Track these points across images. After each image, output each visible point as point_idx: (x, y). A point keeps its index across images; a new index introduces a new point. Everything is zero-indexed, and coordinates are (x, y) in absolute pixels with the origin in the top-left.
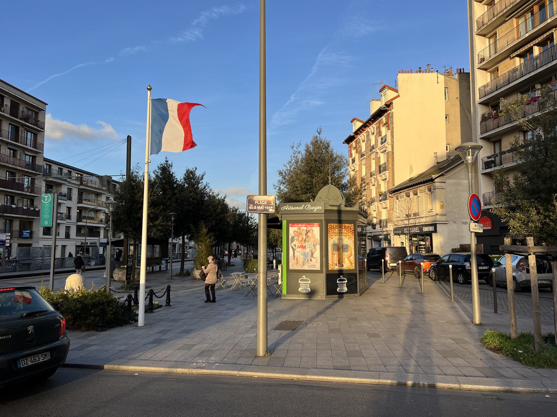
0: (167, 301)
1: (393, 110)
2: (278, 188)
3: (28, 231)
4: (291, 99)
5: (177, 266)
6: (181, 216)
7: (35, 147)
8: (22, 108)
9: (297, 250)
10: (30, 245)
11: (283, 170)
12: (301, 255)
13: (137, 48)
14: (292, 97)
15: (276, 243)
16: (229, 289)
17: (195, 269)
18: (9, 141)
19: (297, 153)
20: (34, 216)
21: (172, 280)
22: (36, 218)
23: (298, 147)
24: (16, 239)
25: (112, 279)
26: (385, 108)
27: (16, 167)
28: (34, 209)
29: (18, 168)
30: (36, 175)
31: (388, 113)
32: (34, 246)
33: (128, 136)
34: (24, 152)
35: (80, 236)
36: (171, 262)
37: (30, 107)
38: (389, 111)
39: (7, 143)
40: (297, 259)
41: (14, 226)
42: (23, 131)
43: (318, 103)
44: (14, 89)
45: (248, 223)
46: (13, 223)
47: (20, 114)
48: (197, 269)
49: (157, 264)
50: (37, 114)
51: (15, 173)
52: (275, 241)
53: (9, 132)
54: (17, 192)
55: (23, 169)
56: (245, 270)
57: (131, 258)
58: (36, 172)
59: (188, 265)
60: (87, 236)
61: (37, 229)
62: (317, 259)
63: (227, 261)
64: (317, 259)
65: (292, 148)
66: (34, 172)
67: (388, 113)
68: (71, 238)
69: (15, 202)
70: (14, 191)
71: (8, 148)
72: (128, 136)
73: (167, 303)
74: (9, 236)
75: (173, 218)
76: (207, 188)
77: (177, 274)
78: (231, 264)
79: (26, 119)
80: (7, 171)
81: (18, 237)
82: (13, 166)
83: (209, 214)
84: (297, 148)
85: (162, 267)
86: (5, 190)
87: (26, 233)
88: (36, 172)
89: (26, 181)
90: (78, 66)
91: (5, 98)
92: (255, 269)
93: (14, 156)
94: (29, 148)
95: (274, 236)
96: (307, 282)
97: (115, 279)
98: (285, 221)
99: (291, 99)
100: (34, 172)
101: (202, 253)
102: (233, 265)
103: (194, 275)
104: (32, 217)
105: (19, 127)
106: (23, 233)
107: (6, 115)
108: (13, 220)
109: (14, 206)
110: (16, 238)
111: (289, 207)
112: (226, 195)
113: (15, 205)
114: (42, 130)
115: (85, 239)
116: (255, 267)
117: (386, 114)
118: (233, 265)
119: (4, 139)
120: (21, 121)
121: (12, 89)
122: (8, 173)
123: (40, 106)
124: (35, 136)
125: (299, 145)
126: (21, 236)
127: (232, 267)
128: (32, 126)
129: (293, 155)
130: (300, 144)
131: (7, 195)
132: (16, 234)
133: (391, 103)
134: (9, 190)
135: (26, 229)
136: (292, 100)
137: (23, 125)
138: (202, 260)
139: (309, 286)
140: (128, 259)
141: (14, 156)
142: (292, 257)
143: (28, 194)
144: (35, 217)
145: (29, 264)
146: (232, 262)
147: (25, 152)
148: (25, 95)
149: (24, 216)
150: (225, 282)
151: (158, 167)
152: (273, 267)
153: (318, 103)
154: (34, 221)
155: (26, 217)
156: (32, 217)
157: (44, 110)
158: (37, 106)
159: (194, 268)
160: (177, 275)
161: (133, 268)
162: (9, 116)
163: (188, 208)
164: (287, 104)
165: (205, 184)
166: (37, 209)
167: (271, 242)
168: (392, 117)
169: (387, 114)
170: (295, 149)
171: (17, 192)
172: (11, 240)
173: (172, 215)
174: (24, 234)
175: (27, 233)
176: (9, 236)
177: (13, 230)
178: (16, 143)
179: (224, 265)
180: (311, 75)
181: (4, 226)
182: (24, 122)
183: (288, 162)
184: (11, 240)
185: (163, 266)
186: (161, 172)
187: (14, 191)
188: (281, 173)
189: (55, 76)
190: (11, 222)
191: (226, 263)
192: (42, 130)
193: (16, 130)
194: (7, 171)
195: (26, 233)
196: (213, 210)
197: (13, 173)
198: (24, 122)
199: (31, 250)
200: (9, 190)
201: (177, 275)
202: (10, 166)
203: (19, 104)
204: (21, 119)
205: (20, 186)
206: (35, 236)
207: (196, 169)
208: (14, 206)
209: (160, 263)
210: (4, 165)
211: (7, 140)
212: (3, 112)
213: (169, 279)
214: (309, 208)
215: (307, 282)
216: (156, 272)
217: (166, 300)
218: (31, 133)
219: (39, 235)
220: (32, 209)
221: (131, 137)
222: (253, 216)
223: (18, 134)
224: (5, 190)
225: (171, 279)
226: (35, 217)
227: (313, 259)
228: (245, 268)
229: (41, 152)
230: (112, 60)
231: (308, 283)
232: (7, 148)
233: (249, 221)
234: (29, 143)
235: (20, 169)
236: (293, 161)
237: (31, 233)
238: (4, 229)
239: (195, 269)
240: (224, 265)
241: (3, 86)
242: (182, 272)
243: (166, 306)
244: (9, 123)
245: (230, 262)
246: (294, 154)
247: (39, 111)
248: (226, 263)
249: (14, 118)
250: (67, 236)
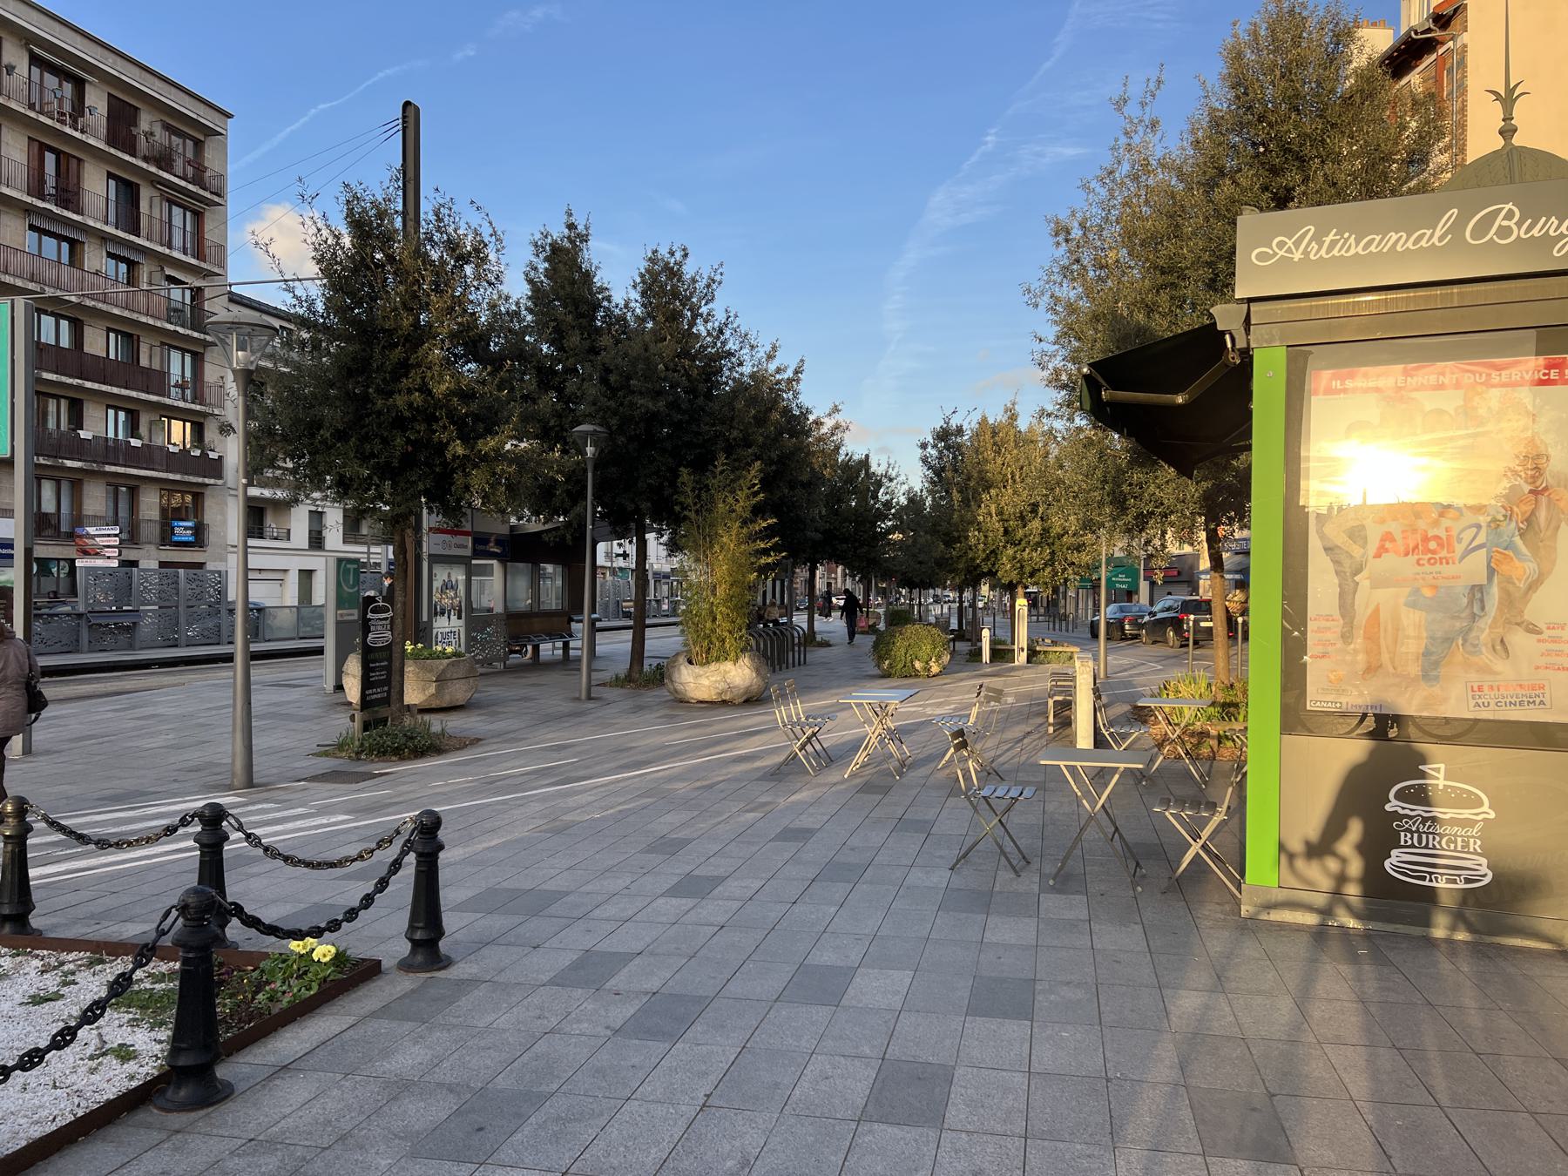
0: (418, 935)
1: (1465, 38)
2: (1046, 298)
3: (189, 524)
4: (986, 143)
5: (616, 645)
6: (621, 440)
7: (199, 255)
8: (146, 121)
9: (1375, 566)
10: (200, 565)
11: (1073, 214)
12: (1413, 605)
13: (538, 13)
14: (989, 138)
15: (994, 565)
16: (833, 776)
17: (682, 659)
18: (110, 229)
19: (1141, 129)
20: (205, 477)
21: (591, 705)
22: (212, 481)
23: (1150, 98)
24: (153, 547)
25: (338, 697)
26: (1429, 30)
27: (135, 316)
28: (204, 455)
29: (143, 319)
30: (206, 344)
31: (1440, 51)
32: (210, 566)
33: (407, 104)
34: (162, 269)
35: (356, 543)
36: (239, 659)
37: (176, 122)
38: (1443, 44)
39: (104, 238)
40: (1372, 637)
41: (143, 507)
42: (157, 201)
43: (1070, 152)
44: (119, 60)
45: (875, 497)
46: (138, 496)
47: (142, 143)
48: (690, 662)
49: (552, 635)
50: (198, 145)
51: (135, 337)
52: (987, 559)
53: (107, 199)
54: (143, 396)
55: (159, 324)
56: (878, 666)
57: (386, 610)
58: (202, 336)
59: (660, 641)
60: (373, 544)
61: (219, 517)
62: (1555, 640)
63: (805, 626)
64: (1555, 640)
65: (1119, 109)
66: (196, 335)
67: (1440, 51)
68: (327, 548)
69: (143, 430)
70: (134, 394)
71: (110, 255)
72: (407, 104)
73: (416, 944)
74: (116, 535)
75: (590, 450)
76: (727, 333)
77: (617, 678)
78: (819, 638)
79: (164, 161)
80: (109, 330)
81: (158, 540)
82: (126, 314)
83: (735, 433)
84: (1143, 104)
85: (572, 644)
86: (104, 388)
87: (183, 531)
88: (202, 336)
89: (178, 366)
90: (381, 75)
91: (87, 86)
92: (918, 665)
93: (132, 280)
94: (177, 254)
95: (986, 537)
96: (1466, 814)
97: (350, 699)
98: (1280, 354)
99: (986, 143)
100: (196, 335)
101: (714, 594)
102: (826, 644)
103: (680, 687)
104: (200, 480)
105: (138, 185)
106: (173, 528)
107: (92, 141)
108: (137, 487)
109: (135, 442)
110: (150, 543)
111: (1318, 238)
112: (802, 361)
113: (140, 438)
114: (216, 199)
115: (369, 553)
116: (920, 654)
117: (1429, 59)
118: (826, 644)
119: (91, 223)
120: (144, 165)
121: (111, 58)
122: (112, 335)
123: (208, 119)
124: (198, 216)
125: (1152, 86)
126: (166, 537)
127: (823, 652)
128: (183, 183)
129: (1123, 140)
130: (1159, 82)
131: (117, 409)
132: (150, 531)
133: (1456, 10)
134: (115, 390)
135: (184, 516)
136: (990, 145)
137: (155, 181)
138: (709, 624)
139: (1475, 845)
140: (370, 615)
141: (132, 280)
142: (1328, 618)
143: (181, 404)
144: (207, 481)
145: (131, 629)
146: (821, 632)
147: (166, 269)
148: (156, 80)
149: (171, 476)
150: (814, 734)
151: (536, 245)
152: (977, 654)
153: (1070, 152)
154: (208, 492)
155: (178, 477)
156: (200, 480)
157: (222, 134)
158: (194, 116)
159: (677, 654)
160: (618, 682)
161: (396, 655)
162: (102, 145)
163: (650, 405)
164: (974, 159)
165: (720, 317)
166: (212, 455)
167: (973, 559)
168: (1462, 64)
169: (1434, 56)
170: (1132, 110)
171: (143, 396)
172: (123, 550)
173: (587, 433)
174: (177, 531)
175: (186, 528)
176: (116, 535)
177: (85, 513)
178: (132, 238)
179: (796, 640)
180: (1048, 65)
181: (111, 505)
182: (153, 169)
183: (1099, 173)
184: (123, 550)
185: (578, 645)
186: (547, 265)
187: (134, 394)
188: (1062, 231)
189: (321, 106)
190: (133, 492)
191: (801, 632)
192: (216, 199)
193: (128, 193)
194: (109, 330)
195: (183, 531)
196: (754, 417)
197: (130, 335)
198: (153, 169)
199: (135, 579)
200: (115, 390)
201: (618, 682)
202: (116, 311)
203: (137, 109)
204: (146, 159)
205: (156, 380)
206: (212, 537)
207: (686, 255)
208: (135, 442)
209: (563, 633)
210: (94, 309)
211: (99, 225)
212: (83, 132)
213: (578, 699)
214: (1504, 232)
215: (1466, 814)
216: (551, 665)
217: (412, 927)
218: (185, 208)
219: (225, 537)
220: (197, 453)
221: (417, 110)
222: (896, 470)
223: (138, 207)
224: (104, 388)
225: (589, 698)
226: (207, 481)
227: (1518, 639)
228: (881, 659)
229: (216, 270)
230: (472, 53)
231: (1472, 823)
232: (104, 254)
233: (882, 490)
234: (177, 240)
235: (151, 322)
236: (1125, 168)
237: (199, 531)
238: (111, 513)
239: (682, 659)
240: (796, 640)
241: (79, 47)
242: (636, 668)
243: (406, 966)
244: (109, 173)
245: (814, 633)
246: (1126, 133)
247: (206, 135)
248: (801, 632)
249: (120, 154)
250: (317, 541)
